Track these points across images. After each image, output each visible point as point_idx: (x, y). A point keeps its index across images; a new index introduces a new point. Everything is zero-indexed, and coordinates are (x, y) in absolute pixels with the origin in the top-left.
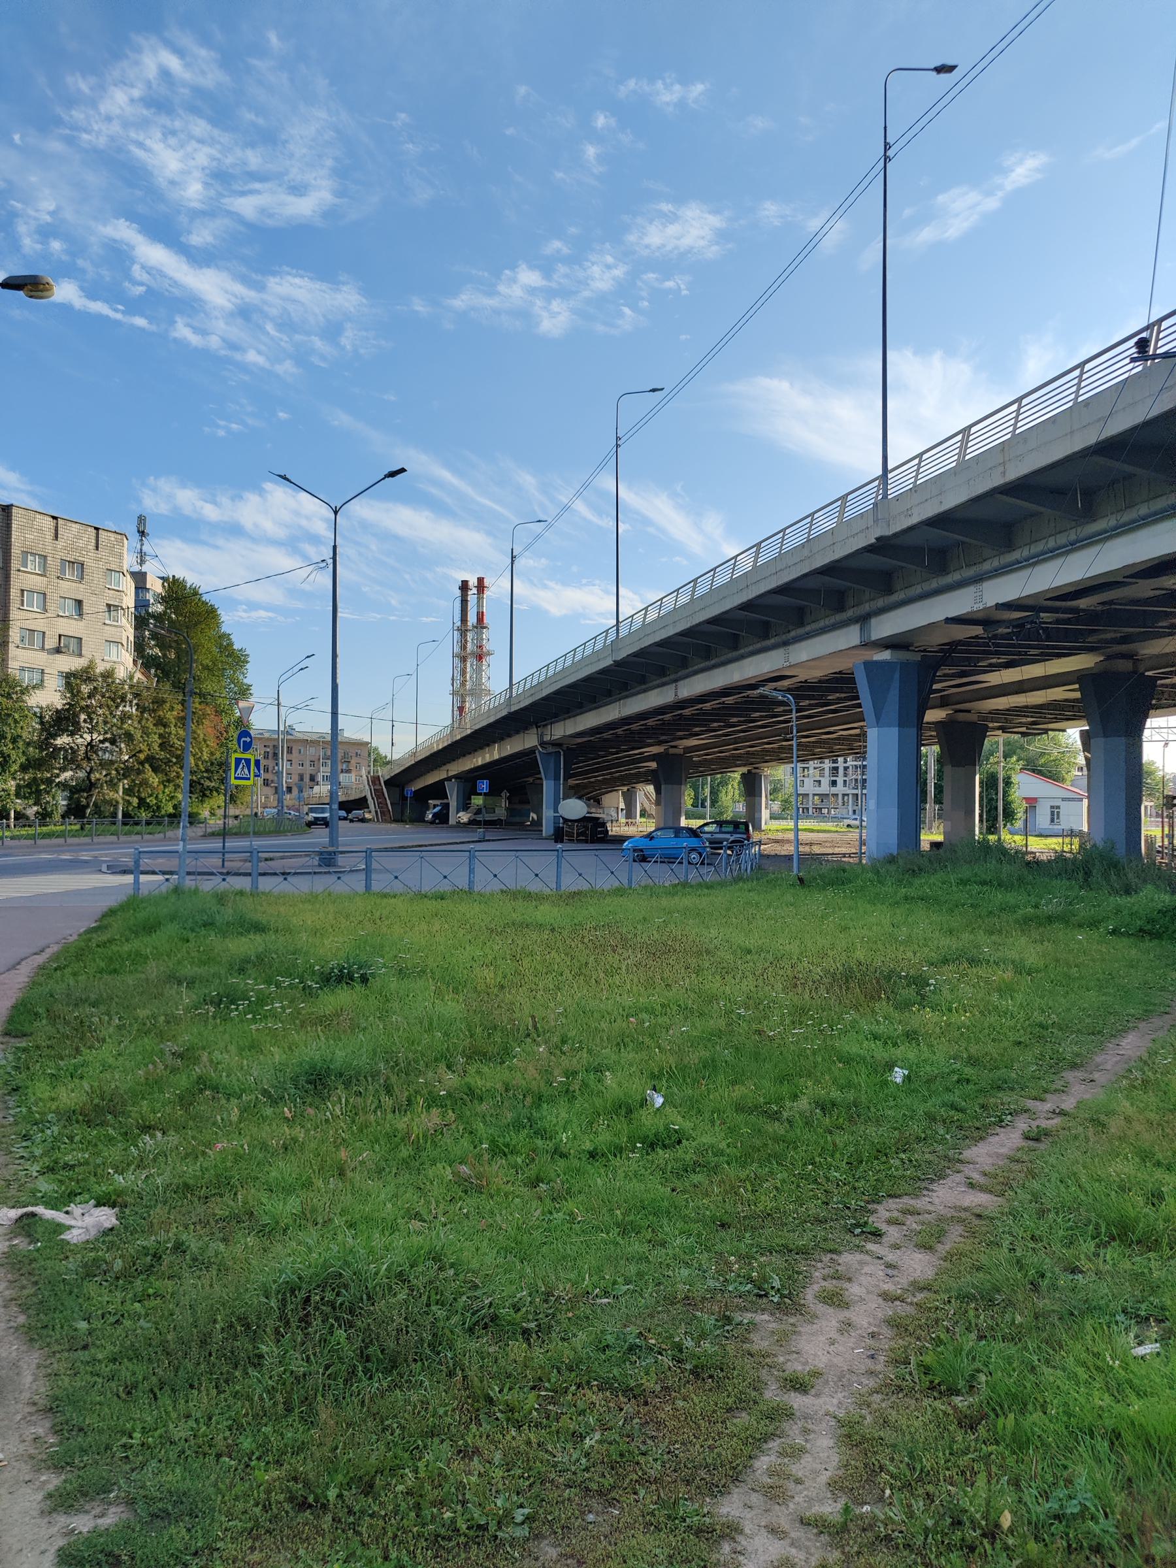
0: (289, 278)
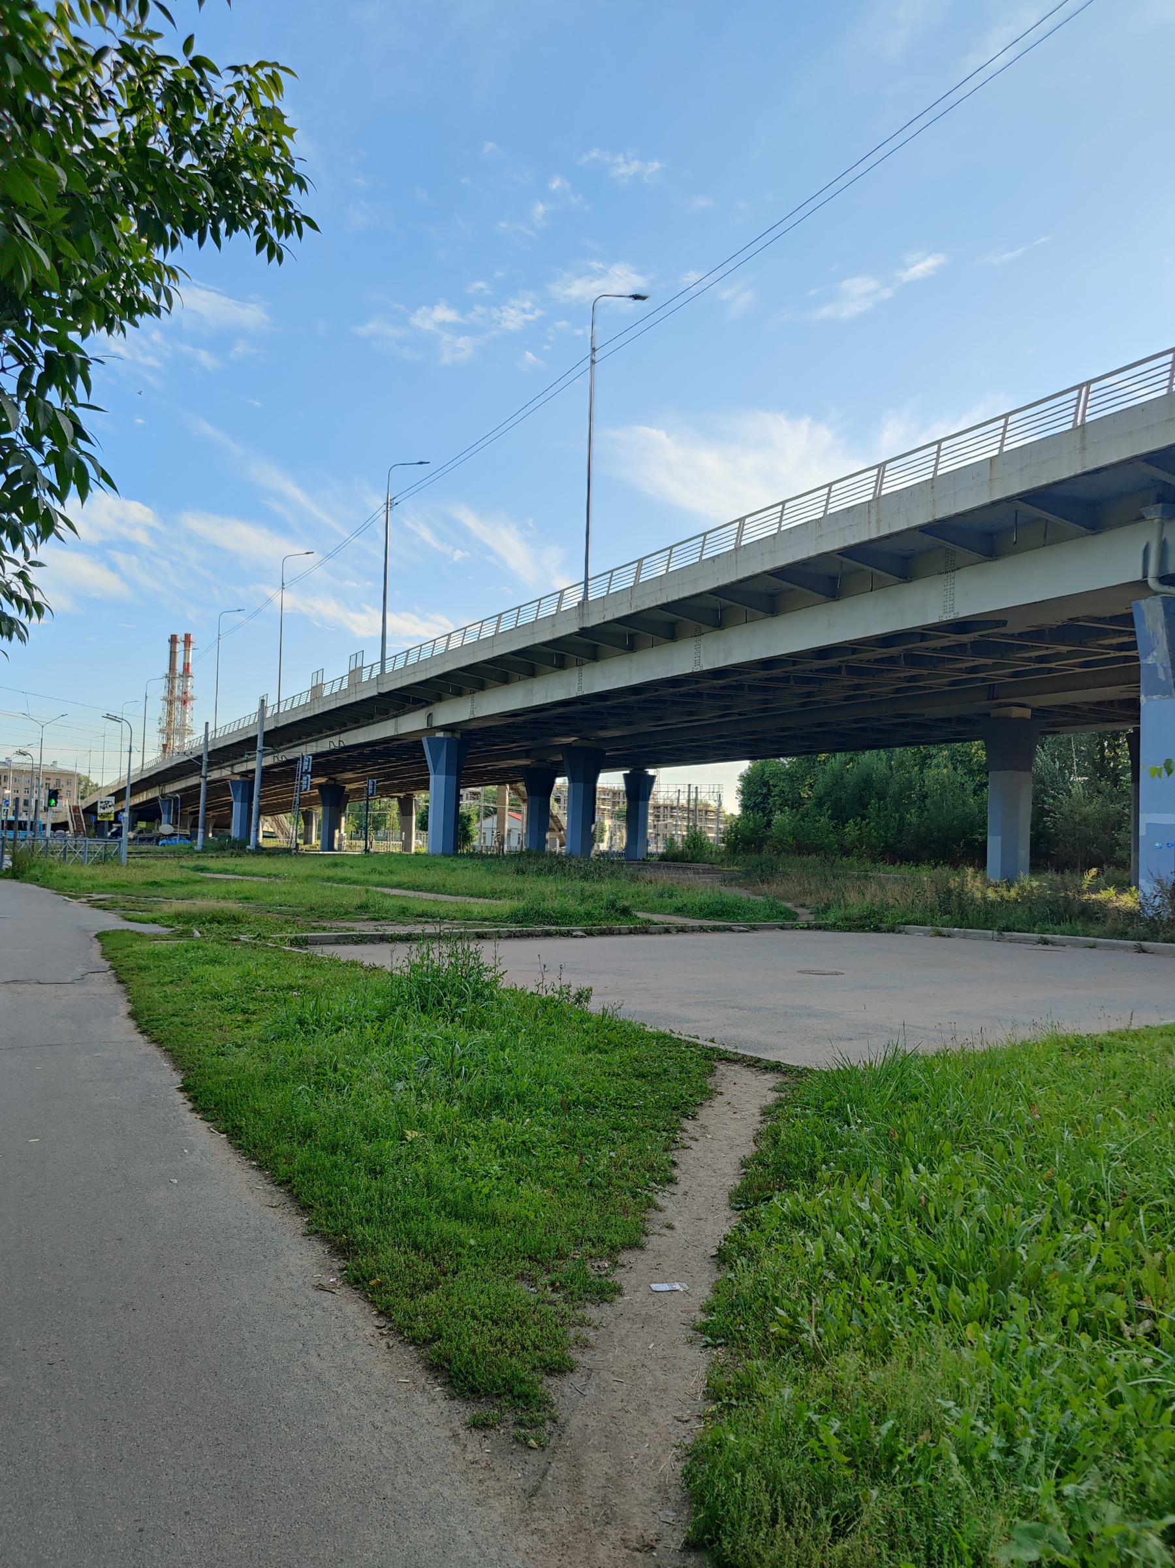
0: (196, 289)
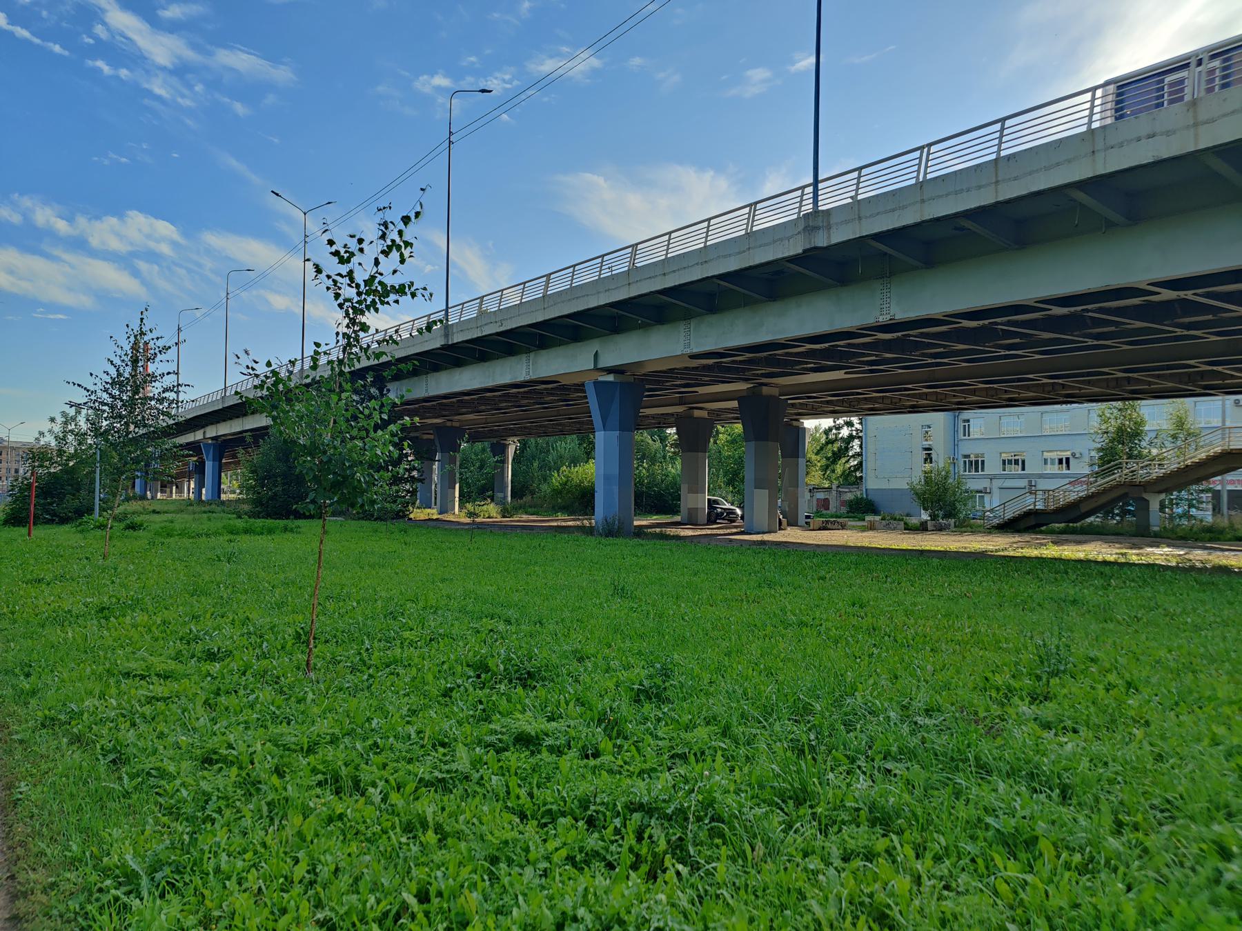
0: (239, 53)
